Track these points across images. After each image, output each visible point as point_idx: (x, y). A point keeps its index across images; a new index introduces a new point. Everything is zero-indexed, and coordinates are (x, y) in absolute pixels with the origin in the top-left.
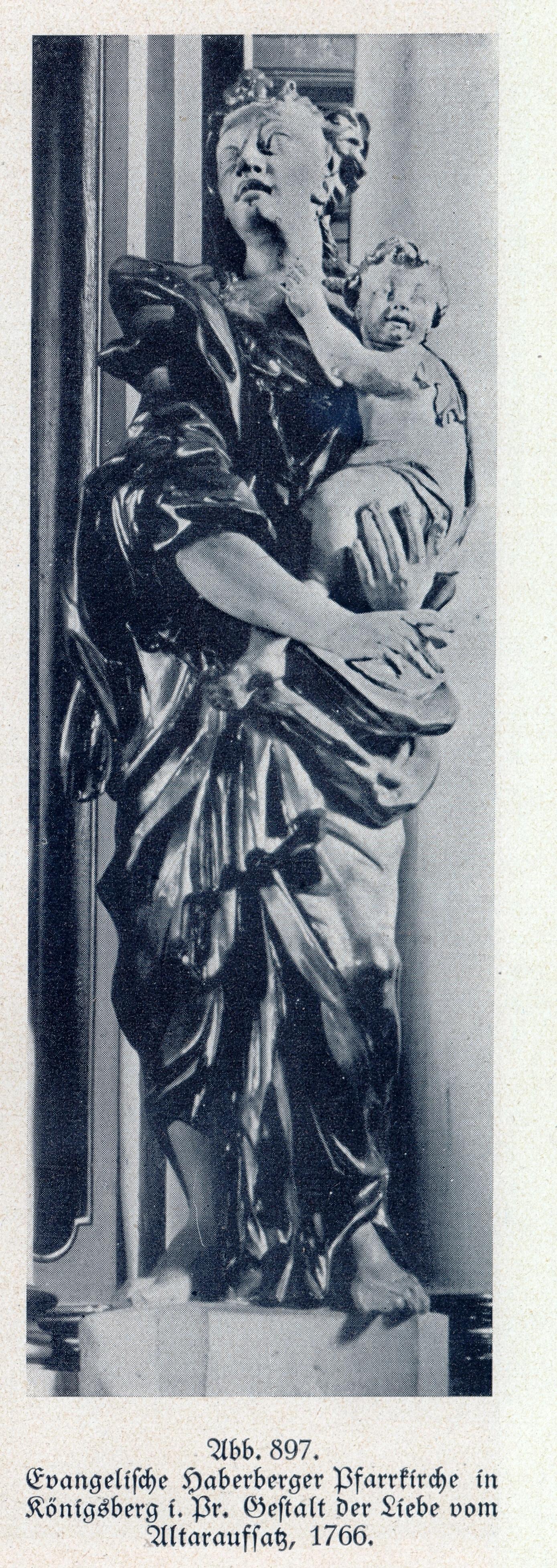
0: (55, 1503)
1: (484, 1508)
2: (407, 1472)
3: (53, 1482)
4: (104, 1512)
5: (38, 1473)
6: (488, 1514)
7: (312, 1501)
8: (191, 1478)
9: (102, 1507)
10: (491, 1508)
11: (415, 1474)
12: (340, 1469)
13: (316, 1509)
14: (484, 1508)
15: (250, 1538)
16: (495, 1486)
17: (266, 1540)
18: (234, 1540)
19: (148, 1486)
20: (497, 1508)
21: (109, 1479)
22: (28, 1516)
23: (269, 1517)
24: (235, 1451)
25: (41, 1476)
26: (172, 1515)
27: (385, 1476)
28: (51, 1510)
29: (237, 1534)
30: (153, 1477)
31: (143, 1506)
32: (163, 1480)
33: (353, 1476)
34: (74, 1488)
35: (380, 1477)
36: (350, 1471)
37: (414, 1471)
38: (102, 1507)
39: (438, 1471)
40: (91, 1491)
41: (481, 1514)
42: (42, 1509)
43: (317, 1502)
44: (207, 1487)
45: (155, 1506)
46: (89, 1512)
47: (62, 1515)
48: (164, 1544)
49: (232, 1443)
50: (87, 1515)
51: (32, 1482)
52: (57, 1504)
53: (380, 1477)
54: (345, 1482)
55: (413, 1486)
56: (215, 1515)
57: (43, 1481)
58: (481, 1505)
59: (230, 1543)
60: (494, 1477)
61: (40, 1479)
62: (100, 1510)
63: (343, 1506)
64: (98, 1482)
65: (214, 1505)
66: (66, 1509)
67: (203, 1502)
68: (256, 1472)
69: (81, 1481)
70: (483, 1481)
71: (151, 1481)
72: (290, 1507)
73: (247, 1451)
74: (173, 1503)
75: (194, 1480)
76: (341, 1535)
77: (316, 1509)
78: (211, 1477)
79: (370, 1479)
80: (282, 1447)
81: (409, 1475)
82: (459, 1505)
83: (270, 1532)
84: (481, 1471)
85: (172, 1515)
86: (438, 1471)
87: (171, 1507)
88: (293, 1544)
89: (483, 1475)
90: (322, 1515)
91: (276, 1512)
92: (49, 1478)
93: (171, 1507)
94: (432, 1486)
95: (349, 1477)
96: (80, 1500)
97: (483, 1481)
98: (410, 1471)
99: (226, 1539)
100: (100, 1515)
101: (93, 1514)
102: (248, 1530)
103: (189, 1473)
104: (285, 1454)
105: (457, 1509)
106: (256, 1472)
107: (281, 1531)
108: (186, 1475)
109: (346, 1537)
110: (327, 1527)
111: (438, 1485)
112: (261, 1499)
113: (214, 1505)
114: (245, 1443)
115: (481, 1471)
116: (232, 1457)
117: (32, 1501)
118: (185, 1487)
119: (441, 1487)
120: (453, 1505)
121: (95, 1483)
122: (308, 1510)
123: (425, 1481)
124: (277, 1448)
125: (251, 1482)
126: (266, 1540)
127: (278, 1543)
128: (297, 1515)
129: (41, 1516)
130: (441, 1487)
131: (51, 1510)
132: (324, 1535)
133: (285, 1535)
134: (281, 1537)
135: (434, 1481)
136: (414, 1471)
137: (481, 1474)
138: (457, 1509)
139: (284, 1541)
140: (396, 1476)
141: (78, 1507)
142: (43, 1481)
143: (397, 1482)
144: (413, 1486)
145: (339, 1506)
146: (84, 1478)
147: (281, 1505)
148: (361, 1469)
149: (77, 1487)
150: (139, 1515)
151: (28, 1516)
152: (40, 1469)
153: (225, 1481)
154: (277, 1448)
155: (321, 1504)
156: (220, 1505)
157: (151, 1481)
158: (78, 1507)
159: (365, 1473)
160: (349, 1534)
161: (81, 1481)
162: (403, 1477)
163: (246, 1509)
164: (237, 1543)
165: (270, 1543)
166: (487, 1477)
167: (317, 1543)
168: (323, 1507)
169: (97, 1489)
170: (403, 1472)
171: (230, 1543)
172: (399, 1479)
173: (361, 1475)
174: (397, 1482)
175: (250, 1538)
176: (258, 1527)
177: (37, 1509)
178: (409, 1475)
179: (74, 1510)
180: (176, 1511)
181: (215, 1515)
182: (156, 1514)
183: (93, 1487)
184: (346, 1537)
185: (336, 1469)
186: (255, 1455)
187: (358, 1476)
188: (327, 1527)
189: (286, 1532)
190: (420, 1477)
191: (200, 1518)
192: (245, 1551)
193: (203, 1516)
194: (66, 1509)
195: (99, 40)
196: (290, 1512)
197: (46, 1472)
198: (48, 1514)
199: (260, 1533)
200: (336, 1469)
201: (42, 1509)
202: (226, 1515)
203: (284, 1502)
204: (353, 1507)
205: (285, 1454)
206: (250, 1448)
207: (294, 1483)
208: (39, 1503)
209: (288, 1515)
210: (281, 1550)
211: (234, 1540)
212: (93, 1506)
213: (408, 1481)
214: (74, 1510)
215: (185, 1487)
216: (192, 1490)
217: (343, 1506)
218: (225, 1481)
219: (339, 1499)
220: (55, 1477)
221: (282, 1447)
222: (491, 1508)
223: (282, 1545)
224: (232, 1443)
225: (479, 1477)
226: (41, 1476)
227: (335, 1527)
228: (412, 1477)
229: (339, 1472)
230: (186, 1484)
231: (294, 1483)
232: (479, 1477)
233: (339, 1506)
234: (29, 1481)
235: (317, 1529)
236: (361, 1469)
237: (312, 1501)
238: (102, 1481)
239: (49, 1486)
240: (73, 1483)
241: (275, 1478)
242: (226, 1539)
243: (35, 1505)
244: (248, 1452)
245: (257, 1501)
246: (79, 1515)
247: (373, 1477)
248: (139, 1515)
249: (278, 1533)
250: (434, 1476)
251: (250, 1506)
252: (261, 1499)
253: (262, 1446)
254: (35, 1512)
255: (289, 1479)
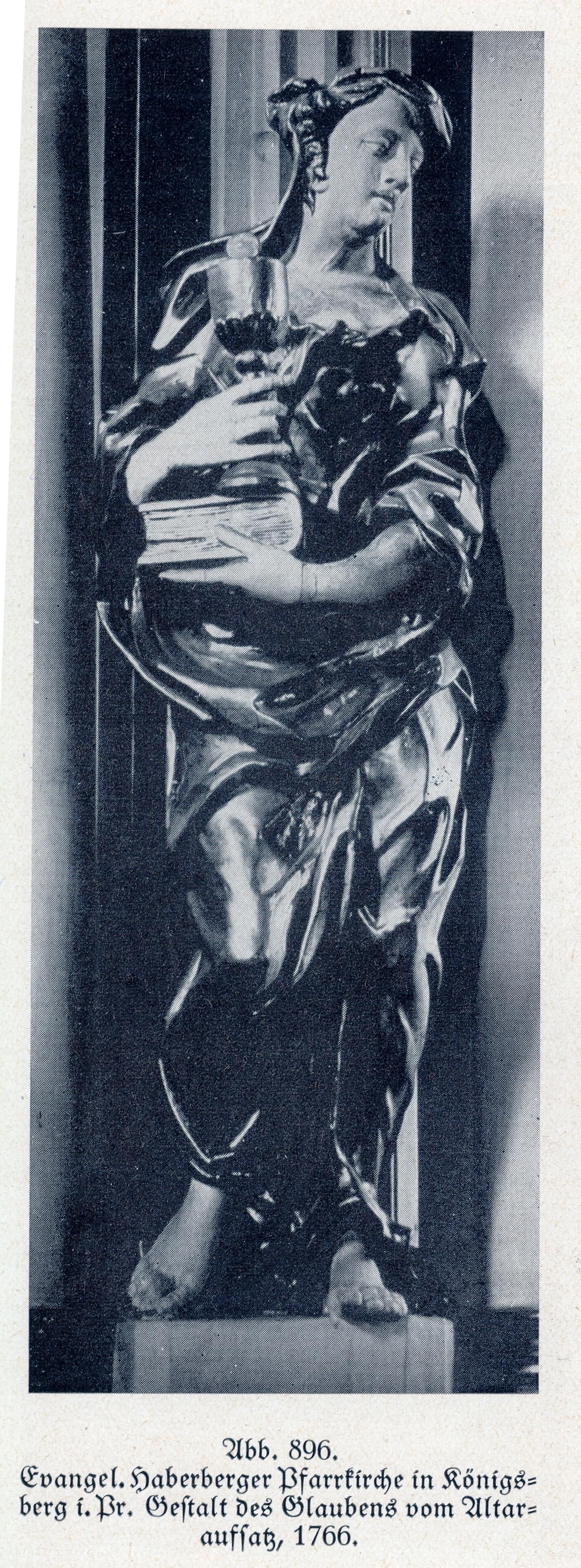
0: (471, 1474)
1: (440, 1509)
2: (352, 1472)
3: (47, 1480)
4: (520, 1484)
5: (33, 1471)
6: (444, 1515)
7: (213, 1500)
8: (138, 1477)
9: (519, 1479)
10: (447, 1509)
11: (361, 1475)
12: (284, 1469)
13: (218, 1509)
14: (440, 1509)
15: (238, 1537)
16: (431, 1487)
17: (254, 1539)
18: (221, 1539)
19: (383, 1487)
20: (453, 1509)
21: (256, 1479)
22: (445, 1487)
23: (360, 1517)
24: (251, 1452)
25: (36, 1474)
26: (80, 1513)
27: (331, 1477)
28: (468, 1481)
29: (225, 1533)
30: (387, 1477)
31: (51, 1504)
32: (398, 1479)
33: (297, 1476)
34: (68, 1487)
35: (326, 1477)
36: (294, 1470)
37: (360, 1472)
38: (519, 1479)
39: (383, 1471)
40: (501, 1491)
41: (437, 1515)
42: (459, 1480)
43: (218, 1502)
44: (155, 1486)
45: (64, 1504)
46: (505, 1484)
47: (479, 1486)
48: (239, 1457)
49: (247, 1443)
50: (503, 1487)
51: (26, 1480)
52: (474, 1475)
53: (326, 1477)
54: (289, 1482)
55: (358, 1486)
56: (120, 1514)
57: (37, 1479)
58: (437, 1506)
59: (218, 1542)
60: (430, 1478)
61: (34, 1476)
62: (517, 1482)
63: (242, 1507)
64: (509, 1483)
65: (119, 1505)
66: (483, 1480)
67: (107, 1501)
68: (203, 1471)
69: (75, 1479)
70: (419, 1482)
71: (386, 1482)
72: (192, 1506)
73: (262, 1451)
74: (81, 1502)
75: (141, 1478)
76: (325, 1534)
77: (218, 1509)
78: (158, 1476)
79: (202, 1508)
80: (301, 1447)
81: (355, 1475)
82: (415, 1506)
83: (258, 1532)
84: (417, 1472)
85: (80, 1513)
86: (383, 1471)
87: (79, 1505)
88: (281, 1542)
89: (419, 1476)
90: (223, 1514)
91: (179, 1511)
92: (43, 1476)
93: (79, 1505)
94: (377, 1486)
95: (293, 1477)
96: (496, 1472)
97: (419, 1482)
98: (355, 1471)
99: (328, 1510)
100: (517, 1487)
101: (509, 1486)
102: (235, 1529)
103: (137, 1472)
104: (303, 1454)
105: (413, 1510)
106: (203, 1471)
107: (269, 1531)
108: (133, 1474)
109: (329, 1537)
110: (311, 1527)
111: (383, 1487)
112: (163, 1498)
113: (119, 1505)
114: (260, 1443)
115: (417, 1472)
116: (248, 1457)
117: (449, 1472)
118: (132, 1486)
119: (386, 1488)
120: (409, 1506)
121: (90, 1482)
122: (209, 1510)
123: (370, 1482)
124: (296, 1448)
125: (199, 1482)
126: (254, 1539)
127: (267, 1544)
128: (505, 1516)
129: (458, 1487)
130: (386, 1488)
131: (468, 1481)
132: (308, 1536)
133: (273, 1535)
134: (269, 1538)
135: (379, 1482)
136: (360, 1472)
137: (417, 1474)
138: (413, 1510)
139: (272, 1541)
140: (341, 1477)
141: (494, 1478)
142: (37, 1479)
143: (342, 1482)
144: (358, 1486)
145: (238, 1507)
146: (79, 1477)
147: (184, 1504)
148: (306, 1469)
149: (72, 1485)
150: (47, 1514)
151: (445, 1487)
152: (35, 1467)
153: (172, 1480)
154: (296, 1448)
155: (223, 1504)
156: (124, 1504)
157: (386, 1482)
158: (494, 1478)
159: (310, 1474)
160: (333, 1534)
161: (75, 1479)
162: (348, 1477)
163: (285, 1509)
164: (225, 1543)
165: (258, 1543)
166: (423, 1477)
167: (300, 1543)
168: (225, 1507)
169: (244, 1488)
170: (348, 1472)
171: (218, 1542)
172: (345, 1479)
173: (306, 1476)
174: (342, 1482)
175: (238, 1537)
176: (246, 1526)
177: (453, 1480)
178: (355, 1475)
179: (490, 1482)
180: (83, 1511)
181: (120, 1514)
182: (64, 1512)
183: (88, 1485)
184: (329, 1537)
185: (280, 1469)
186: (271, 1454)
187: (302, 1476)
188: (311, 1527)
189: (274, 1532)
190: (365, 1477)
191: (104, 1516)
192: (233, 1549)
193: (107, 1515)
194: (483, 1480)
195: (383, 38)
196: (192, 1512)
197: (41, 1471)
198: (465, 1485)
199: (248, 1532)
200: (280, 1469)
201: (459, 1480)
202: (130, 1514)
203: (187, 1502)
204: (252, 1507)
205: (303, 1454)
206: (266, 1448)
207: (243, 1483)
208: (455, 1475)
209: (191, 1514)
210: (269, 1550)
211: (221, 1539)
212: (509, 1478)
213: (352, 1482)
214: (490, 1482)
215: (132, 1486)
216: (140, 1489)
217: (242, 1507)
218: (172, 1480)
219: (238, 1500)
220: (49, 1476)
221: (301, 1447)
222: (447, 1509)
223: (271, 1546)
224: (247, 1443)
225: (415, 1478)
226: (36, 1474)
227: (319, 1527)
228: (358, 1477)
229: (284, 1472)
230: (134, 1484)
231: (243, 1483)
232: (415, 1478)
233: (238, 1507)
234: (23, 1479)
235: (300, 1529)
236: (306, 1469)
237: (213, 1500)
238: (97, 1480)
239: (43, 1485)
240: (68, 1481)
241: (40, 1505)
242: (328, 1510)
243: (452, 1477)
244: (264, 1452)
245: (159, 1500)
246: (495, 1487)
247: (318, 1477)
248: (47, 1514)
249: (266, 1533)
250: (378, 1476)
251: (152, 1505)
252: (163, 1498)
253: (280, 1447)
254: (452, 1483)
255: (237, 1478)
